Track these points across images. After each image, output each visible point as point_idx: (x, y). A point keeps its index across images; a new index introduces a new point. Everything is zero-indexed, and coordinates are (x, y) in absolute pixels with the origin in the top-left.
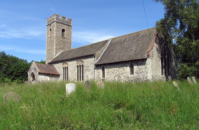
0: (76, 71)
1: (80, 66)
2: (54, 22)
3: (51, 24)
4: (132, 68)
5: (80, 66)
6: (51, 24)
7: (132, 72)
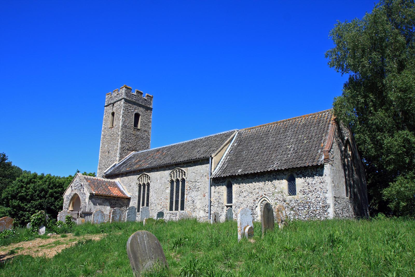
0: (168, 191)
1: (178, 180)
2: (121, 99)
3: (115, 102)
4: (291, 181)
5: (178, 180)
6: (115, 102)
7: (292, 191)
